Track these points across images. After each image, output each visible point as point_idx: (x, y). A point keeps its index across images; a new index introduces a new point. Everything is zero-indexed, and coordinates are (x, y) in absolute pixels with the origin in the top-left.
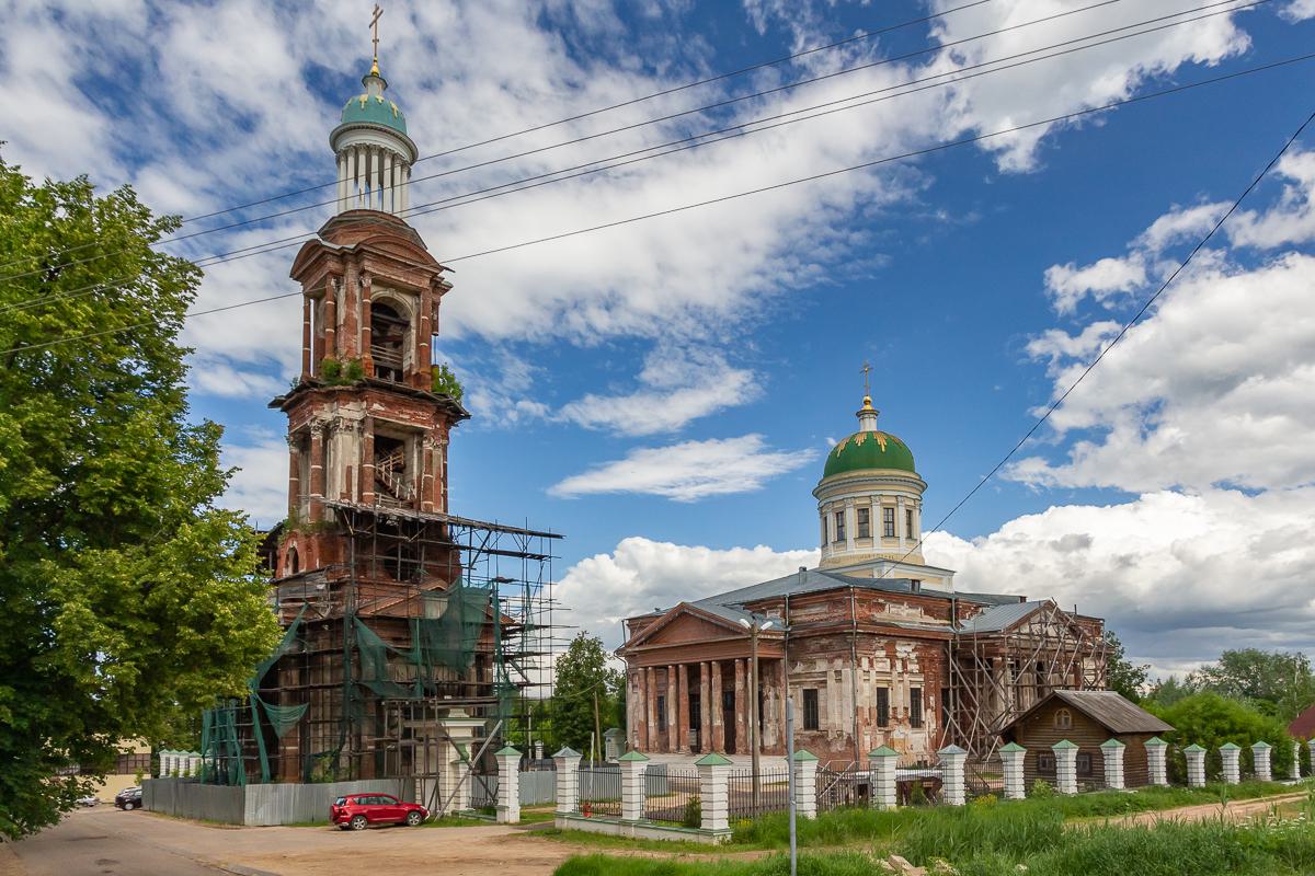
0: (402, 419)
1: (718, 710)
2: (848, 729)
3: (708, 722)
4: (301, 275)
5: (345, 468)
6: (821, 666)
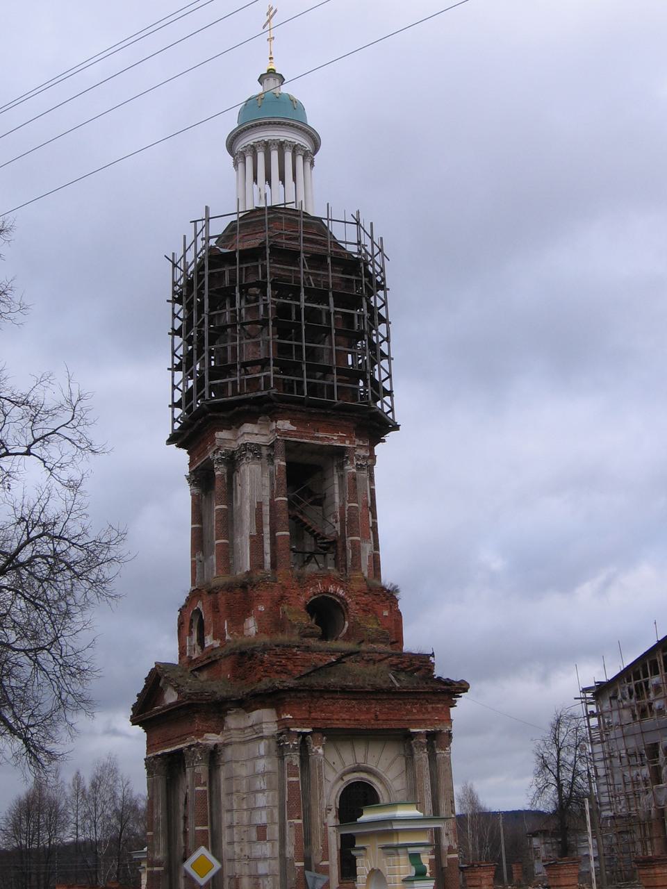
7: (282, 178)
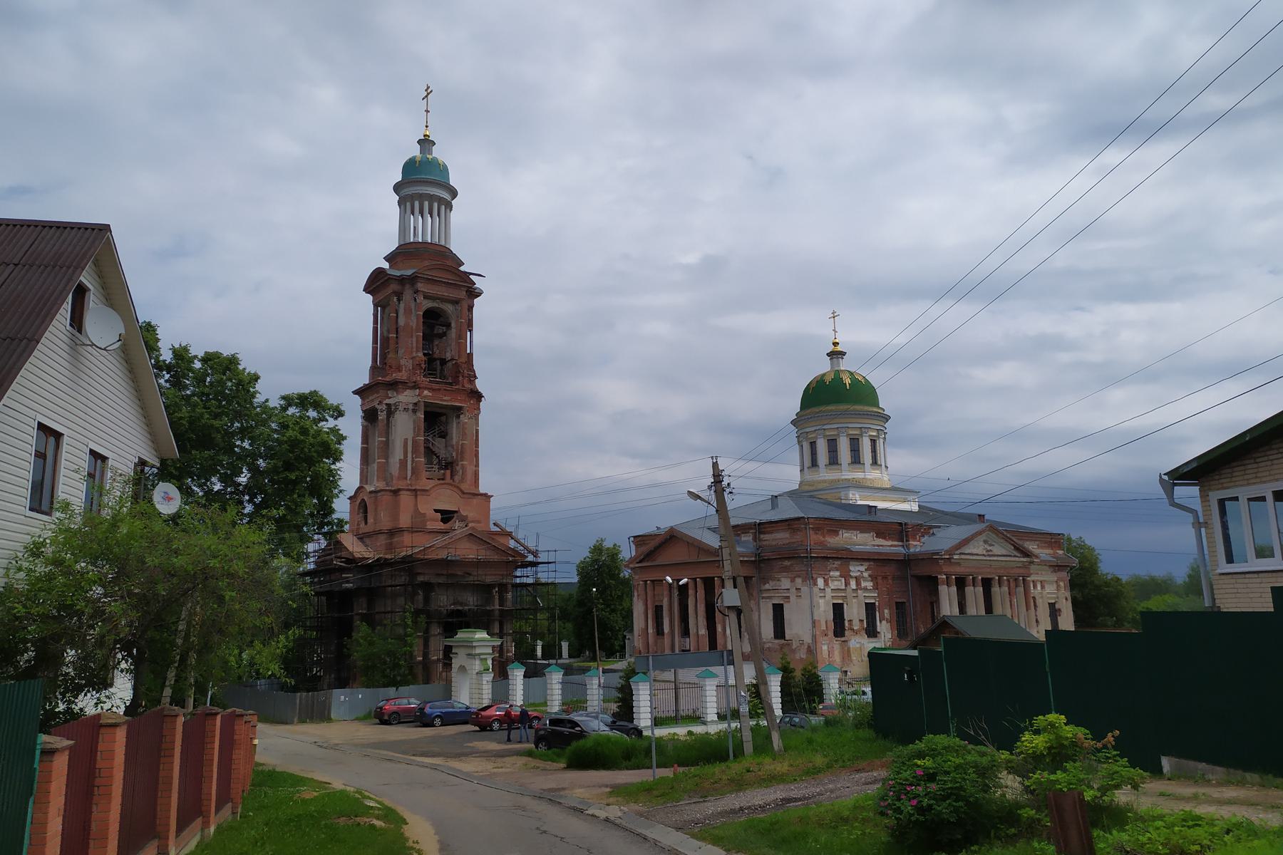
0: (445, 401)
1: (702, 622)
2: (808, 639)
3: (695, 631)
4: (372, 290)
5: (403, 440)
6: (785, 583)
7: (439, 215)
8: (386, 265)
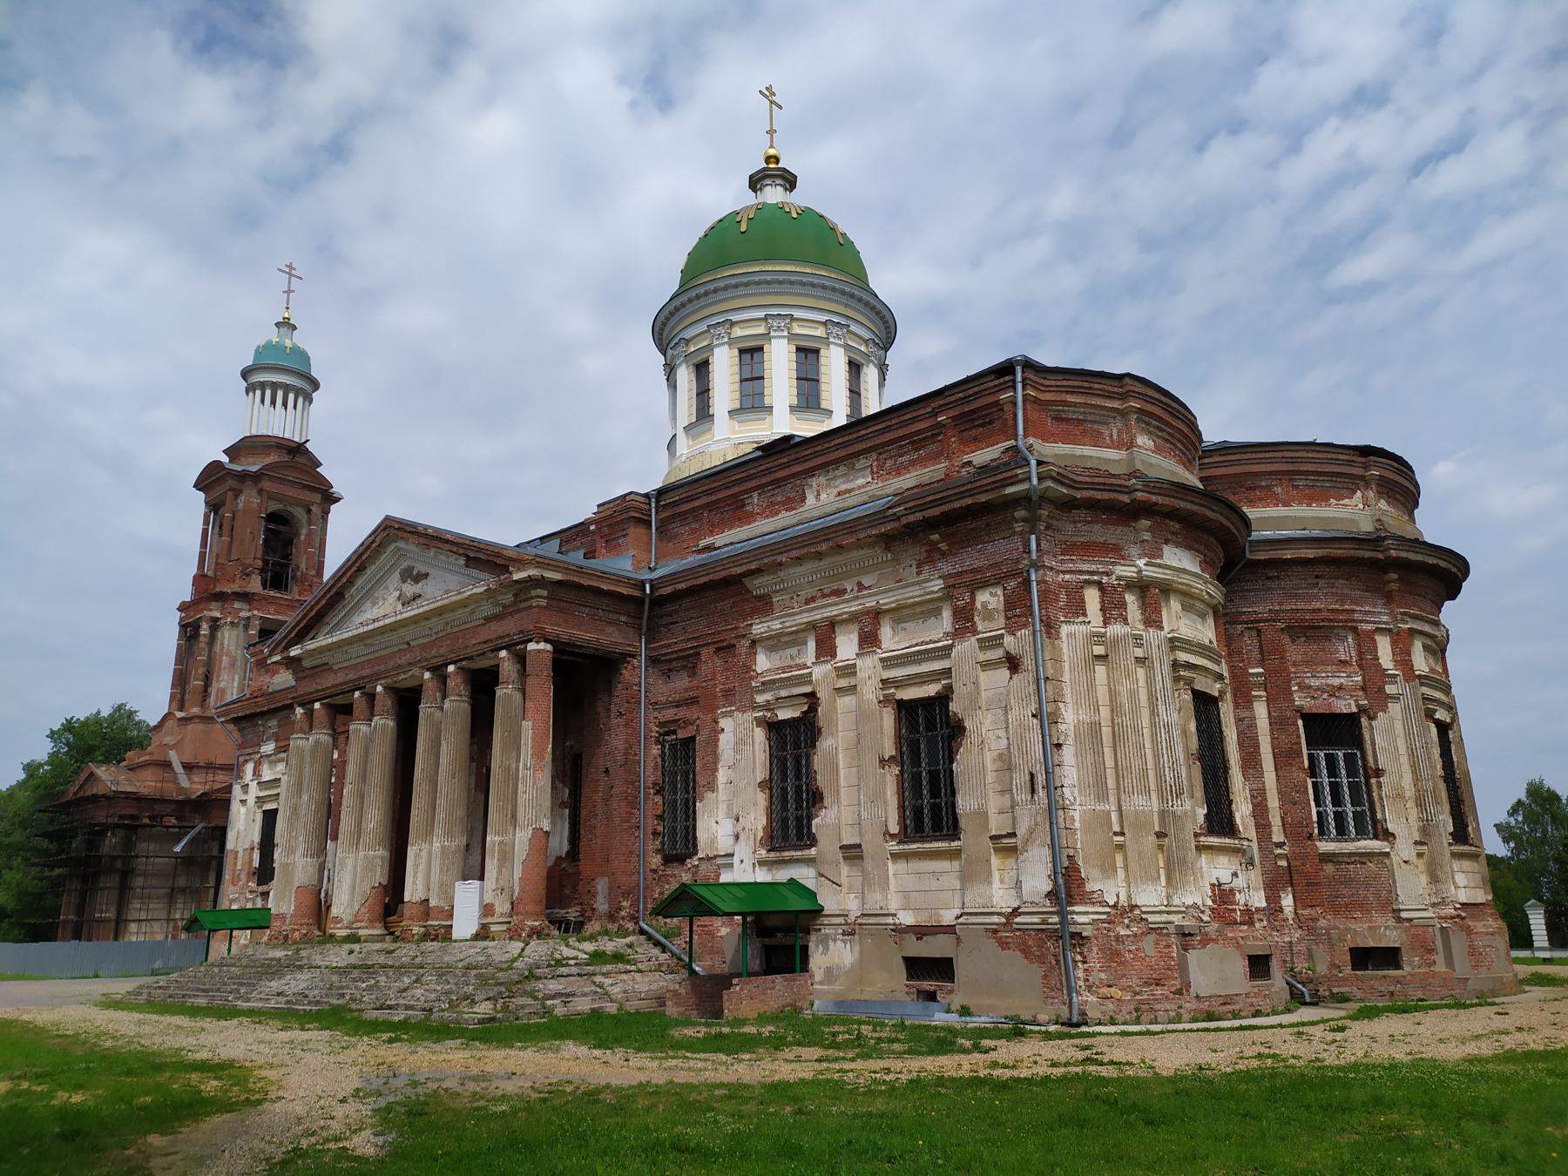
4: (205, 486)
8: (225, 459)
